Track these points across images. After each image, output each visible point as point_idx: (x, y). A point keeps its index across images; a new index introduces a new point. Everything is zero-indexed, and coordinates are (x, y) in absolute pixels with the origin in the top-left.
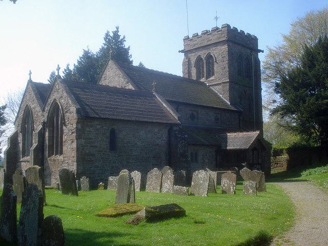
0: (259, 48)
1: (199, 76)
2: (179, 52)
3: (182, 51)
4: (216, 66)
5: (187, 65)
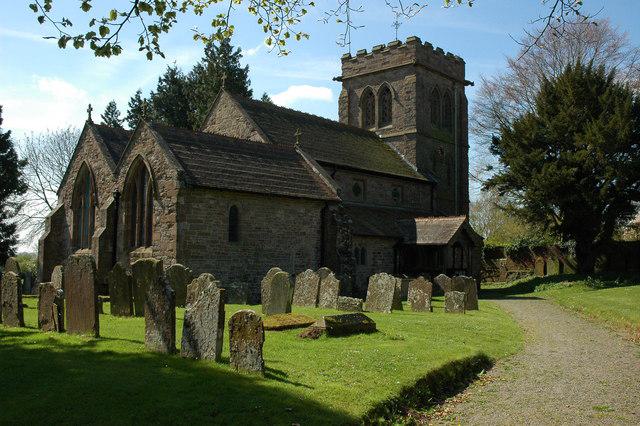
2: (334, 79)
3: (339, 79)
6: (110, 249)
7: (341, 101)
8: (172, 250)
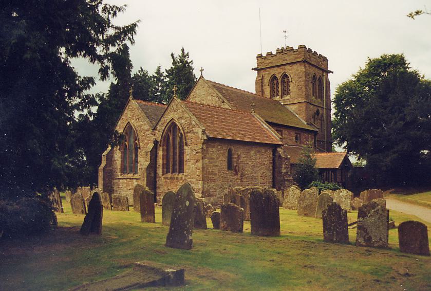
0: (329, 69)
1: (272, 96)
2: (253, 69)
3: (255, 69)
4: (291, 85)
5: (260, 83)
6: (153, 175)
7: (257, 83)
8: (199, 176)
